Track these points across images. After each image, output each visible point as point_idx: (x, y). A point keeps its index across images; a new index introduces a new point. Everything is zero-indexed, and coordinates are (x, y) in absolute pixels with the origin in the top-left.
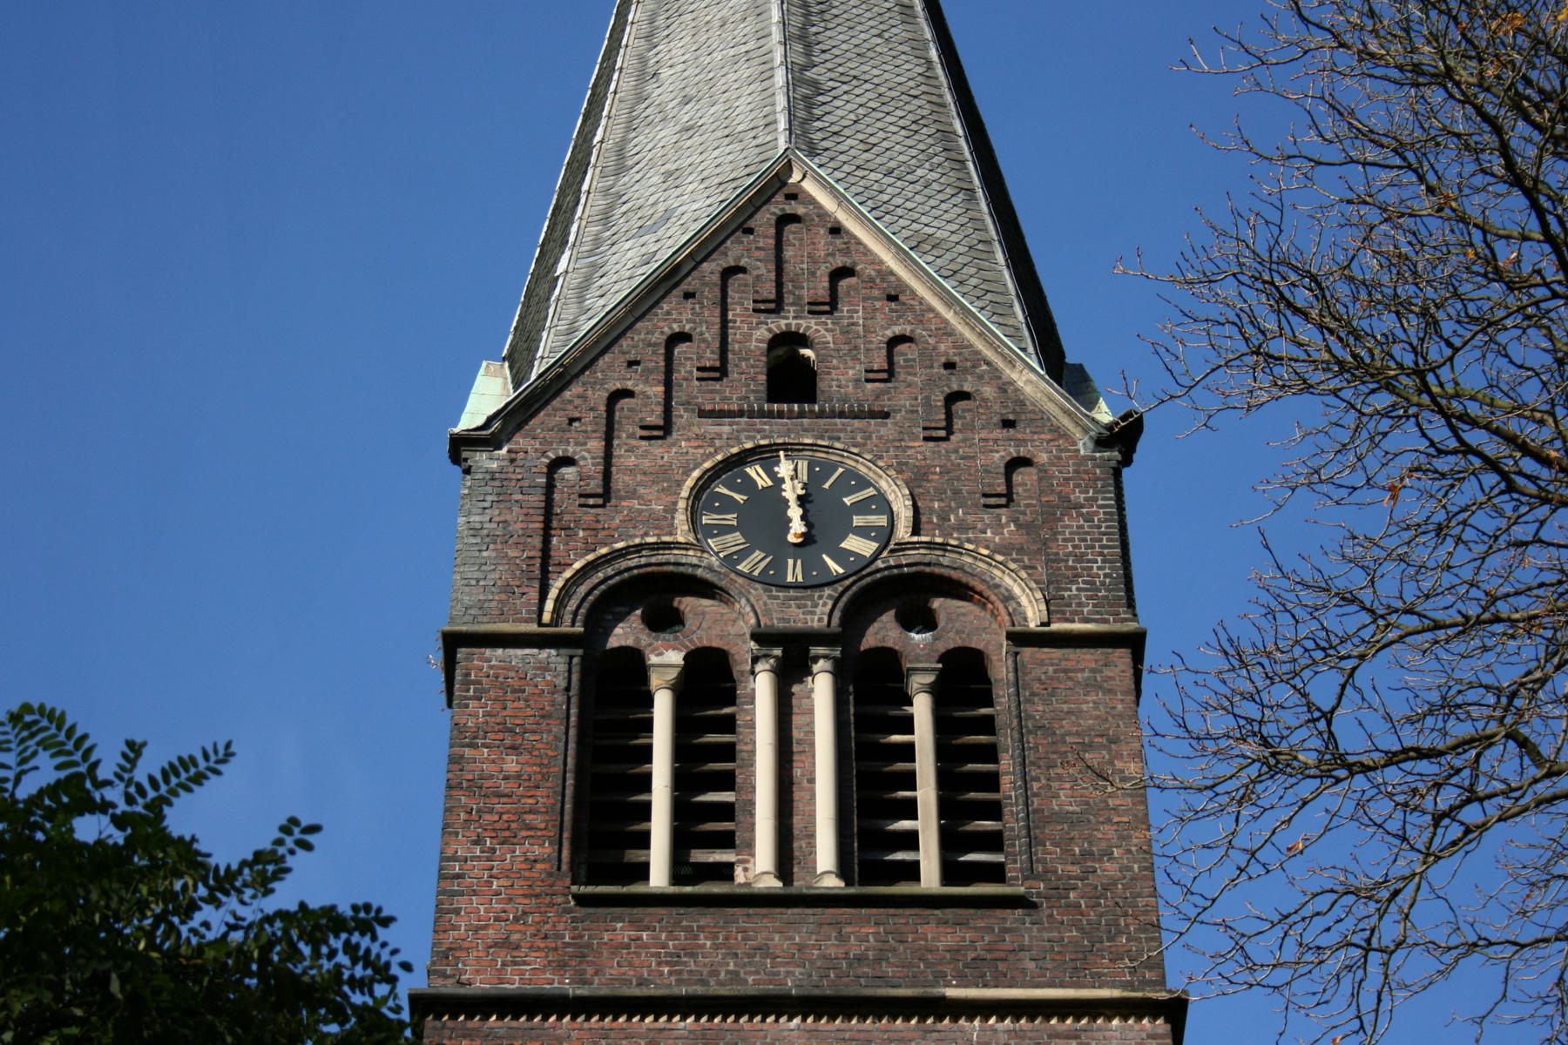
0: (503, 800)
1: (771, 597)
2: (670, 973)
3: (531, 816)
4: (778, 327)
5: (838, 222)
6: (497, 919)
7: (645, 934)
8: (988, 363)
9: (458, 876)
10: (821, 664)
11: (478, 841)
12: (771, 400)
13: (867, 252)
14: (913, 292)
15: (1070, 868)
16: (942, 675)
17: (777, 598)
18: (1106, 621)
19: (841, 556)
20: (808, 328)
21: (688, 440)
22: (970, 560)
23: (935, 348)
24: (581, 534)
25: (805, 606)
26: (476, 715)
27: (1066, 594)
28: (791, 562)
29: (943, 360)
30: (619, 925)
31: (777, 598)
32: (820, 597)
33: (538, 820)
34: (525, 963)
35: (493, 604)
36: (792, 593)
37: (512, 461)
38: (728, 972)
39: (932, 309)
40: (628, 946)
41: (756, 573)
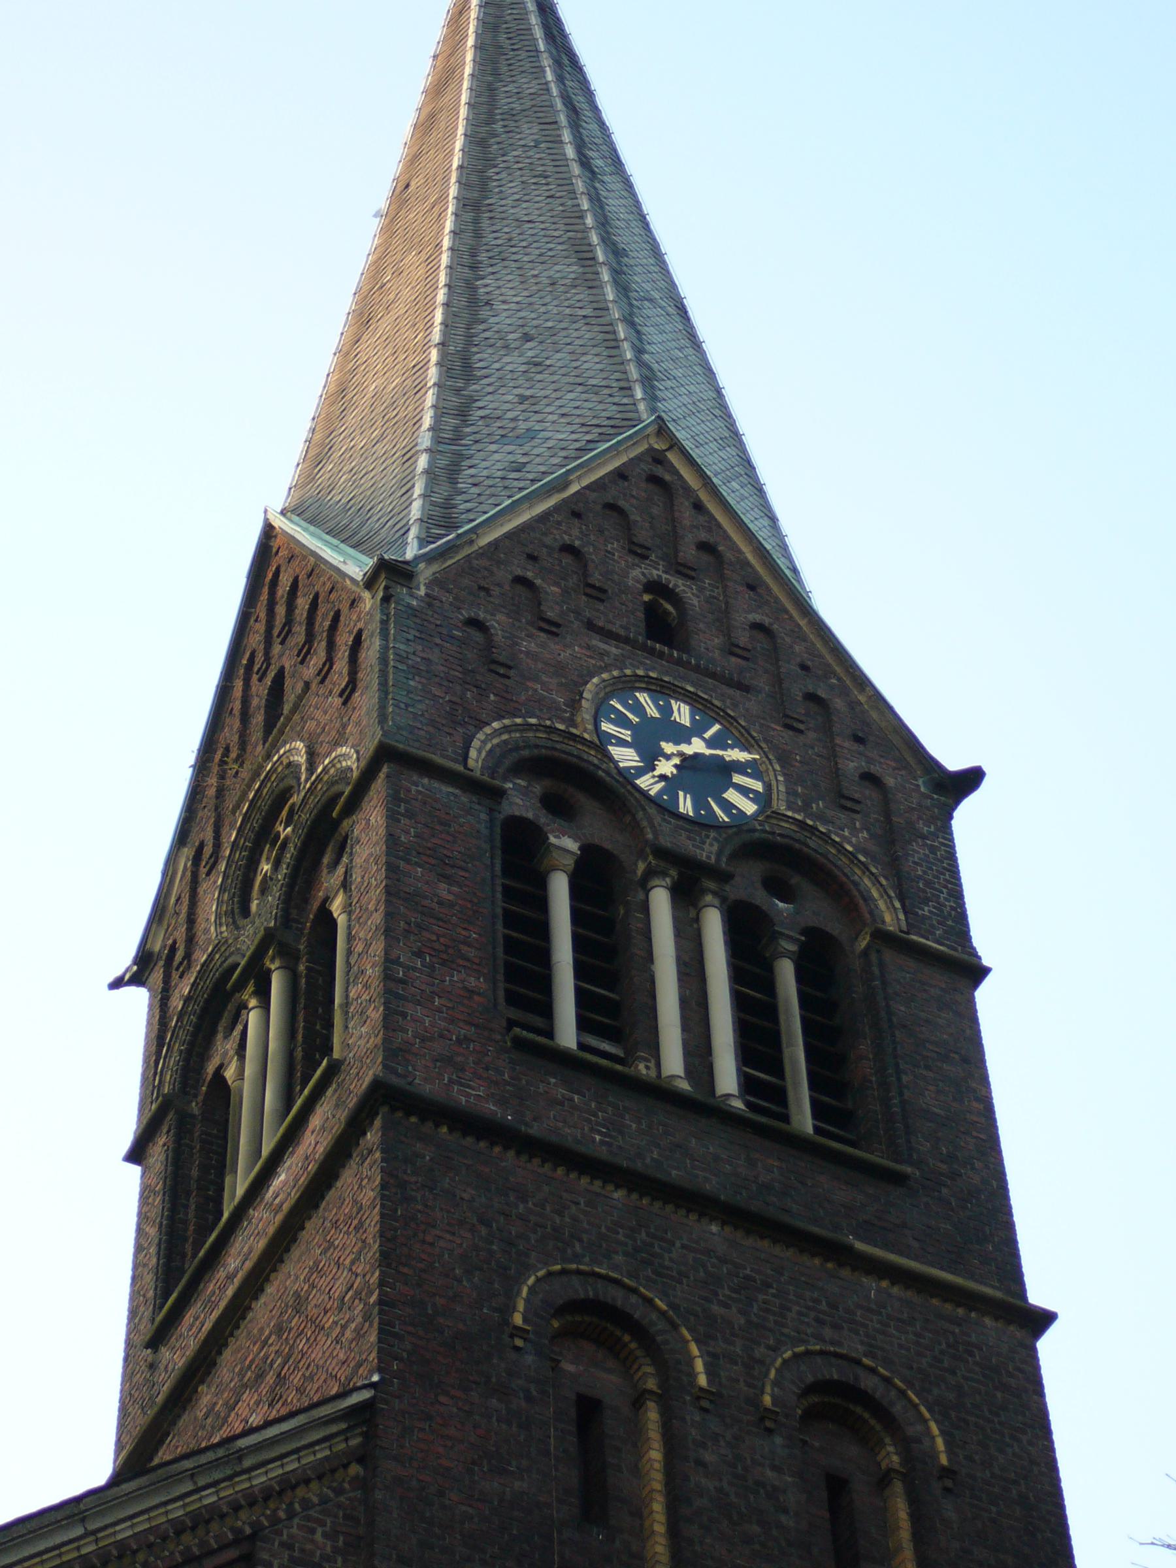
0: (441, 924)
1: (665, 820)
2: (602, 1142)
3: (466, 948)
4: (651, 574)
5: (700, 501)
6: (441, 1036)
7: (576, 1097)
8: (839, 679)
9: (401, 981)
10: (709, 898)
11: (419, 954)
12: (649, 636)
13: (727, 537)
14: (768, 589)
15: (939, 1164)
16: (803, 947)
17: (669, 822)
18: (955, 950)
19: (727, 806)
20: (676, 585)
21: (580, 646)
22: (833, 851)
23: (791, 647)
24: (492, 697)
25: (695, 840)
26: (407, 833)
27: (920, 912)
28: (681, 794)
29: (799, 660)
30: (553, 1080)
31: (669, 822)
32: (708, 837)
33: (471, 953)
34: (469, 1087)
35: (422, 733)
36: (680, 823)
37: (430, 605)
38: (652, 1159)
39: (786, 611)
40: (562, 1104)
41: (758, 786)
